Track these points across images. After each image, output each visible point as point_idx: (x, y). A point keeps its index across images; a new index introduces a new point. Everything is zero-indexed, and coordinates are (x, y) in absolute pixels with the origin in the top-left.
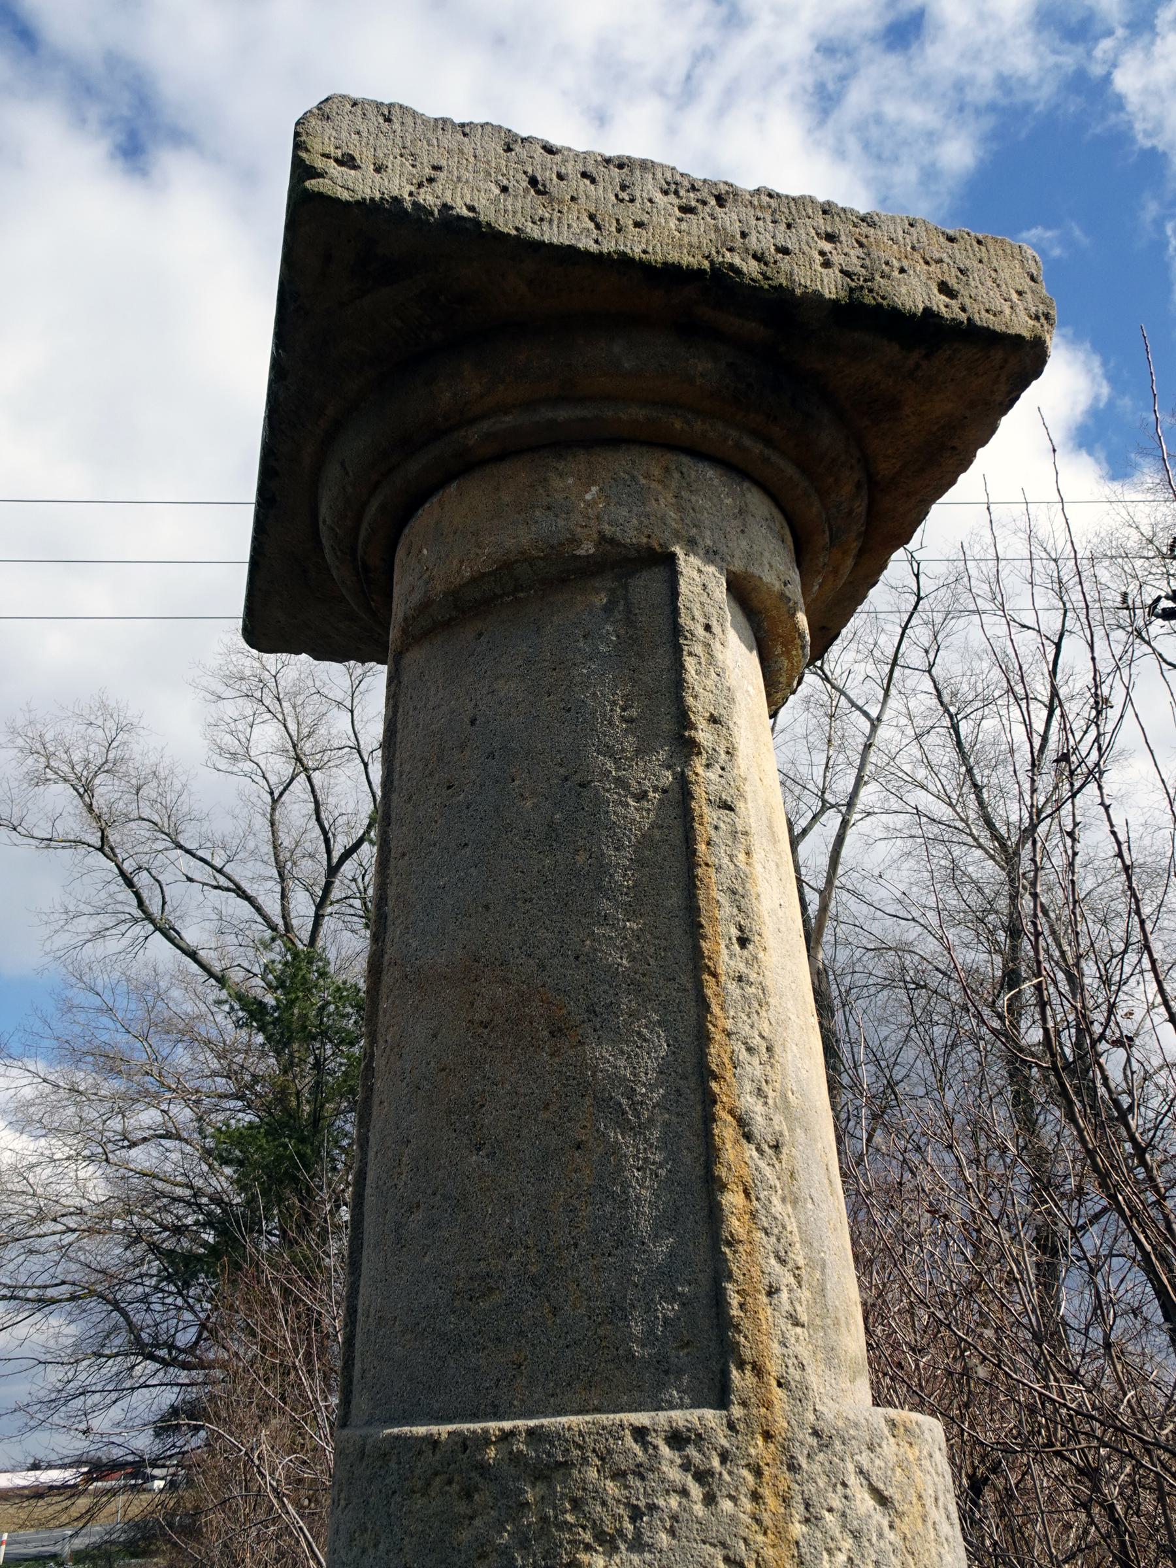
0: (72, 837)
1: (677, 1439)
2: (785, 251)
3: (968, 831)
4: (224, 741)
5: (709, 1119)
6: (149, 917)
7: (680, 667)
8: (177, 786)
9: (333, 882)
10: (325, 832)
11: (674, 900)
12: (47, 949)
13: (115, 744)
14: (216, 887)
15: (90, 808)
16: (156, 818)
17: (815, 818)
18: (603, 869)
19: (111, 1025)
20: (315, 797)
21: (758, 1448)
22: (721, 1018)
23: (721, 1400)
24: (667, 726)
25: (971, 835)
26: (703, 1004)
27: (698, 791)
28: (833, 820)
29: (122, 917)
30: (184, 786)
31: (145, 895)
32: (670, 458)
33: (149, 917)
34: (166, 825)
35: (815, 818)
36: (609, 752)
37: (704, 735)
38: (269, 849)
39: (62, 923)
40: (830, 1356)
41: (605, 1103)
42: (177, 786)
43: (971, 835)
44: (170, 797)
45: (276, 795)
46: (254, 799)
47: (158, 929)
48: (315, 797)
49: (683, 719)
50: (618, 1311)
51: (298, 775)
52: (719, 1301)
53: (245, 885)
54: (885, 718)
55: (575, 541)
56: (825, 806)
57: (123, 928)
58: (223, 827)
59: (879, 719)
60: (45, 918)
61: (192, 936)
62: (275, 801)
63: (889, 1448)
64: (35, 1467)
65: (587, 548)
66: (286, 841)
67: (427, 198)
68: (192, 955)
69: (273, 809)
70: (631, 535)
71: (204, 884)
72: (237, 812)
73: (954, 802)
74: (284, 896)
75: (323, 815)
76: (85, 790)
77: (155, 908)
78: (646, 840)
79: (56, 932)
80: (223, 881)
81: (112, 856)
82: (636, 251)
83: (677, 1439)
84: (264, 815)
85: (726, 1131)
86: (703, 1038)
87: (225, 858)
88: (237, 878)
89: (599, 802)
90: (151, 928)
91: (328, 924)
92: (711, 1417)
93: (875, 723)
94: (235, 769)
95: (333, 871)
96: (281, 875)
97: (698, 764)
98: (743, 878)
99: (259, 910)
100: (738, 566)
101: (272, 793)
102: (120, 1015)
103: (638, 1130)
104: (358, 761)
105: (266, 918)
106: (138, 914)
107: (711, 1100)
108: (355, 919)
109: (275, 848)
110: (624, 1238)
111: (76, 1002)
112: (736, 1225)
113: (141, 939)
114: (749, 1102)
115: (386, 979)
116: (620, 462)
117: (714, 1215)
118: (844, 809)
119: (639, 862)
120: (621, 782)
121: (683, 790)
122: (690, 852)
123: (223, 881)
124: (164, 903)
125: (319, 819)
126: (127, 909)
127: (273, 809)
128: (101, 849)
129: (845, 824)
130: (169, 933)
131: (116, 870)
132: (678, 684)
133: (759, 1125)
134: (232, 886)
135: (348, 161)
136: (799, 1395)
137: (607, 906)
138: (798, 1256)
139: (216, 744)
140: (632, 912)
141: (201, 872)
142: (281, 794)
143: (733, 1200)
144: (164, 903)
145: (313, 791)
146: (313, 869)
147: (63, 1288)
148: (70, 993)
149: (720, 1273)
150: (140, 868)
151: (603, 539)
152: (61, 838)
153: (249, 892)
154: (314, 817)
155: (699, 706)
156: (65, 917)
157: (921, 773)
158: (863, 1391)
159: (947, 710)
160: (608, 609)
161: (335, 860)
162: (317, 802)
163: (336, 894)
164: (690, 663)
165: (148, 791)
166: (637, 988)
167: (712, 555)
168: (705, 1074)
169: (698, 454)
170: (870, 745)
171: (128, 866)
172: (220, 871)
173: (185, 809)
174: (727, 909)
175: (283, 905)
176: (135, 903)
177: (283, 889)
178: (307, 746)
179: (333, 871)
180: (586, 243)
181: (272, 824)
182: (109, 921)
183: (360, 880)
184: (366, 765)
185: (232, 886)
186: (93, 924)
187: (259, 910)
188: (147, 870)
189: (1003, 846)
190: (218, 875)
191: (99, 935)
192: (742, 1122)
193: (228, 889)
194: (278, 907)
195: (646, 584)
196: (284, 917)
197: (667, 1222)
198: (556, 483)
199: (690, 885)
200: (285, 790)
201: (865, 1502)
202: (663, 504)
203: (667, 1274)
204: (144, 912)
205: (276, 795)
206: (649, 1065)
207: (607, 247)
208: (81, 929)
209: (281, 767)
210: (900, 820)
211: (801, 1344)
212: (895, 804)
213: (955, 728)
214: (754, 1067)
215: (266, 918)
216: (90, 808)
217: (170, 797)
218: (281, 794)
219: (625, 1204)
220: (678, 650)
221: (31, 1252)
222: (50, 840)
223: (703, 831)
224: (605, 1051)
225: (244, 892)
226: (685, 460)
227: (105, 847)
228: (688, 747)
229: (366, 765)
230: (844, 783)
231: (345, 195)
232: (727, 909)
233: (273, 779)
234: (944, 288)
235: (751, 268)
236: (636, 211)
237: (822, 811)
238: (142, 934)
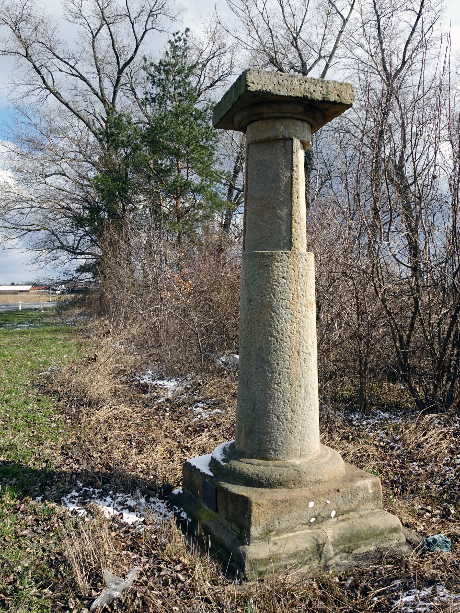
0: (14, 51)
1: (285, 253)
2: (314, 91)
3: (376, 68)
4: (70, 6)
5: (292, 220)
6: (48, 87)
7: (292, 158)
8: (52, 27)
9: (120, 77)
10: (117, 55)
11: (289, 192)
12: (9, 99)
13: (26, 7)
14: (72, 75)
15: (19, 37)
16: (44, 42)
17: (316, 62)
18: (280, 187)
19: (35, 130)
20: (112, 38)
21: (294, 254)
22: (294, 208)
23: (290, 250)
24: (290, 167)
25: (377, 70)
26: (292, 206)
27: (294, 177)
28: (323, 63)
29: (37, 86)
30: (55, 27)
31: (45, 77)
32: (294, 120)
33: (48, 87)
34: (49, 45)
35: (316, 62)
36: (282, 170)
37: (295, 168)
38: (93, 60)
39: (13, 88)
40: (302, 246)
41: (279, 217)
42: (52, 27)
43: (377, 70)
44: (50, 32)
45: (94, 34)
46: (85, 35)
47: (51, 92)
48: (112, 38)
49: (292, 166)
50: (279, 241)
51: (103, 25)
52: (291, 240)
53: (84, 75)
54: (349, 19)
55: (279, 136)
56: (320, 57)
57: (38, 91)
58: (72, 47)
59: (347, 20)
60: (6, 85)
61: (66, 96)
62: (94, 37)
63: (307, 256)
64: (13, 284)
65: (281, 137)
66: (99, 55)
67: (264, 89)
68: (67, 105)
69: (94, 41)
70: (287, 136)
71: (66, 73)
72: (78, 41)
73: (373, 54)
74: (100, 81)
75: (116, 46)
76: (15, 28)
77: (50, 83)
78: (286, 183)
79: (12, 91)
80: (74, 72)
81: (31, 60)
82: (292, 95)
83: (285, 253)
84: (90, 43)
85: (293, 222)
86: (292, 210)
87: (75, 62)
88: (81, 72)
89: (280, 177)
90: (49, 92)
91: (119, 93)
92: (289, 251)
93: (345, 21)
94: (76, 21)
95: (120, 72)
96: (98, 72)
97: (294, 173)
98: (298, 189)
99: (90, 86)
100: (302, 139)
101: (92, 34)
102: (38, 126)
103: (283, 221)
104: (129, 22)
105: (93, 89)
106: (44, 86)
107: (292, 218)
108: (128, 91)
109: (95, 59)
110: (280, 233)
111: (20, 120)
112: (293, 232)
113: (45, 96)
114: (296, 218)
115: (248, 197)
116: (286, 122)
117: (291, 231)
118: (327, 59)
119: (285, 186)
120: (283, 175)
121: (291, 177)
122: (292, 186)
123: (74, 72)
124: (53, 82)
125: (114, 48)
126: (38, 83)
127: (94, 41)
128: (26, 57)
129: (327, 67)
130: (56, 95)
131: (33, 66)
132: (292, 160)
133: (297, 221)
134: (78, 74)
135: (253, 83)
136: (299, 250)
137: (280, 192)
138: (300, 236)
139: (67, 7)
140: (284, 193)
141: (65, 67)
142: (96, 34)
143: (293, 229)
144: (53, 82)
145: (111, 35)
146: (112, 69)
147: (34, 226)
148: (17, 116)
149: (291, 237)
150: (42, 66)
151: (283, 136)
152: (10, 51)
153: (86, 78)
154: (112, 47)
155: (295, 164)
156: (13, 85)
157: (362, 40)
158: (306, 250)
159: (376, 12)
160: (283, 146)
161: (121, 67)
162: (113, 41)
163: (122, 81)
164: (294, 157)
165: (41, 29)
166: (284, 203)
167: (298, 138)
168: (291, 215)
169: (298, 119)
170: (342, 32)
171: (37, 64)
172: (73, 68)
173: (56, 38)
174: (296, 194)
175: (100, 85)
176: (41, 80)
177: (100, 78)
178: (107, 13)
179: (120, 72)
180: (286, 95)
181: (93, 48)
182: (31, 88)
183: (129, 74)
184: (133, 24)
185: (78, 74)
186: (25, 89)
187: (90, 86)
188: (45, 67)
189: (387, 74)
190: (72, 69)
191: (28, 94)
192: (295, 221)
193: (77, 76)
194: (98, 86)
195: (289, 142)
196: (101, 90)
197: (286, 231)
198: (277, 125)
199: (291, 190)
200: (98, 32)
201: (304, 260)
202: (292, 130)
203: (285, 237)
204: (46, 85)
205: (94, 34)
206: (285, 213)
207: (289, 95)
208: (21, 91)
209: (95, 22)
210: (350, 61)
211: (299, 245)
212: (349, 55)
213: (378, 21)
214: (297, 214)
215: (93, 89)
216: (19, 37)
217: (50, 32)
218: (96, 34)
219: (281, 229)
220: (292, 155)
221: (21, 213)
222: (5, 51)
223: (294, 183)
224: (279, 211)
225: (84, 78)
226: (296, 121)
227: (27, 56)
228: (293, 170)
229: (133, 24)
230: (329, 47)
231: (253, 90)
232: (296, 194)
233: (93, 27)
234: (338, 96)
235: (309, 95)
236: (293, 87)
237: (319, 59)
238: (45, 94)
